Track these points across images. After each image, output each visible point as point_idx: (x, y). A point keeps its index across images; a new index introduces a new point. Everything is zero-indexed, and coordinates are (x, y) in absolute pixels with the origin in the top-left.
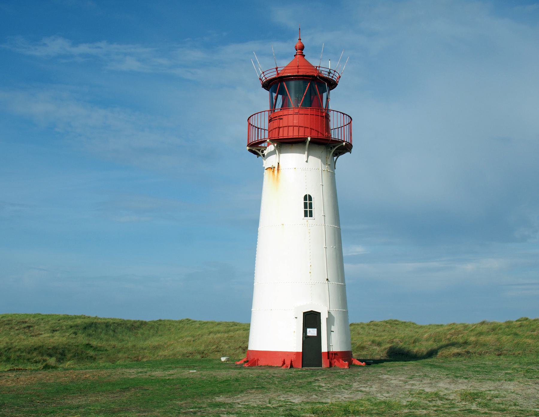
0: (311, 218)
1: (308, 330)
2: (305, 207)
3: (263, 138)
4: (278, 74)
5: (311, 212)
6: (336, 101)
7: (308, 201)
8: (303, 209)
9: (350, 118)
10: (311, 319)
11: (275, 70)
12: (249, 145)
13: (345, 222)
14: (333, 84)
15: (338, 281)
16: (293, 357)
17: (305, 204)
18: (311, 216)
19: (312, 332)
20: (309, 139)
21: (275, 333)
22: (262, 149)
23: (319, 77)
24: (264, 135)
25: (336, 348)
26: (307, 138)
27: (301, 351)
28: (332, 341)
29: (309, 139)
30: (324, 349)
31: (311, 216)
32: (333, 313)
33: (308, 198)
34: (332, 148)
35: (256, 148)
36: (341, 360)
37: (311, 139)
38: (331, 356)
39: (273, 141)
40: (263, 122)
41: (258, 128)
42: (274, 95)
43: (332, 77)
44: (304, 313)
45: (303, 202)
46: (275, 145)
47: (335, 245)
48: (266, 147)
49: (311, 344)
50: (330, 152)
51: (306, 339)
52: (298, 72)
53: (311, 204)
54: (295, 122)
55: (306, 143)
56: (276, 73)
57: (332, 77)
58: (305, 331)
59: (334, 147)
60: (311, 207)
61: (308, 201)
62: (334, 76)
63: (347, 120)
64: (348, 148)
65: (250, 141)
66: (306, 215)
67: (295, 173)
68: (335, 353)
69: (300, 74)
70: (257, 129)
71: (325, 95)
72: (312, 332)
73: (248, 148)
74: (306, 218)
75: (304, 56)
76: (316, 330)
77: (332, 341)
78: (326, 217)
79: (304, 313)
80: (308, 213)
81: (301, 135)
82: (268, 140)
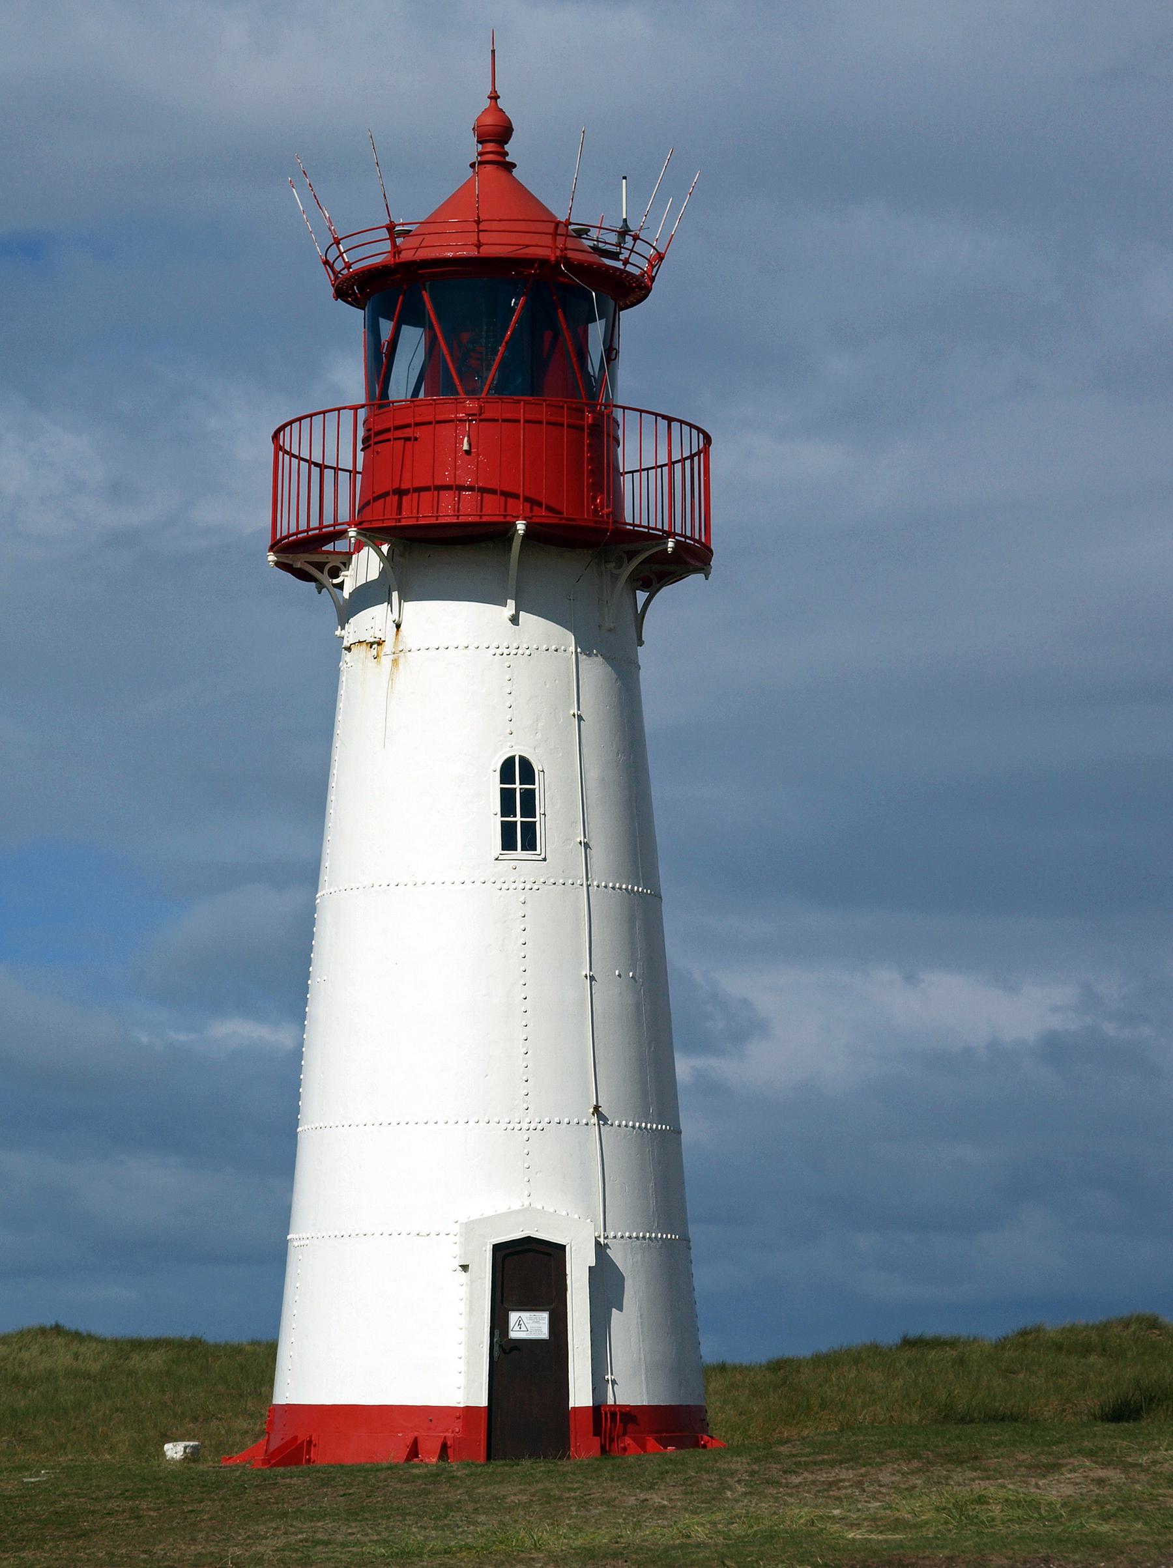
0: (527, 854)
1: (514, 1316)
2: (507, 807)
3: (328, 519)
4: (396, 250)
5: (530, 833)
6: (644, 359)
7: (517, 786)
8: (499, 819)
9: (699, 430)
10: (525, 1270)
11: (384, 234)
12: (277, 546)
13: (663, 889)
14: (631, 290)
15: (645, 1117)
16: (452, 1433)
17: (507, 799)
18: (530, 844)
19: (530, 1325)
20: (521, 526)
21: (380, 1324)
22: (335, 562)
23: (569, 263)
24: (341, 503)
25: (630, 1391)
26: (515, 525)
27: (483, 1402)
28: (611, 1364)
29: (521, 526)
30: (580, 1395)
31: (530, 844)
32: (616, 1254)
33: (517, 773)
34: (619, 565)
35: (307, 555)
36: (651, 1442)
37: (527, 526)
38: (606, 1424)
39: (372, 534)
40: (341, 444)
41: (322, 467)
42: (386, 327)
43: (626, 262)
44: (497, 1248)
45: (495, 786)
46: (385, 548)
47: (633, 967)
48: (349, 555)
49: (523, 1373)
50: (615, 578)
51: (507, 1357)
52: (479, 245)
53: (529, 798)
54: (464, 456)
55: (511, 540)
56: (387, 246)
57: (626, 262)
58: (499, 1323)
59: (631, 555)
60: (529, 808)
61: (517, 786)
62: (634, 259)
63: (697, 443)
64: (693, 557)
65: (288, 525)
66: (508, 843)
67: (445, 691)
68: (628, 1416)
69: (486, 251)
70: (315, 471)
71: (596, 330)
72: (530, 1325)
73: (272, 557)
74: (511, 854)
75: (514, 166)
76: (545, 1315)
77: (611, 1364)
78: (597, 854)
79: (497, 1248)
80: (519, 833)
81: (492, 510)
82: (352, 533)
